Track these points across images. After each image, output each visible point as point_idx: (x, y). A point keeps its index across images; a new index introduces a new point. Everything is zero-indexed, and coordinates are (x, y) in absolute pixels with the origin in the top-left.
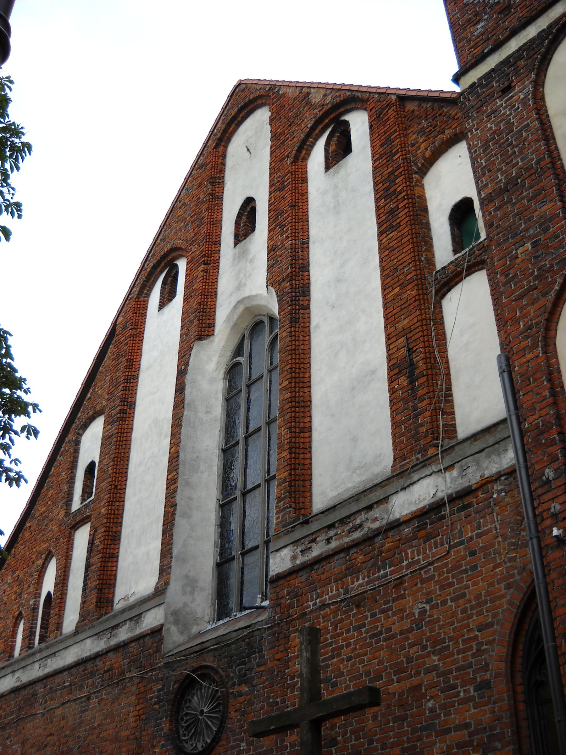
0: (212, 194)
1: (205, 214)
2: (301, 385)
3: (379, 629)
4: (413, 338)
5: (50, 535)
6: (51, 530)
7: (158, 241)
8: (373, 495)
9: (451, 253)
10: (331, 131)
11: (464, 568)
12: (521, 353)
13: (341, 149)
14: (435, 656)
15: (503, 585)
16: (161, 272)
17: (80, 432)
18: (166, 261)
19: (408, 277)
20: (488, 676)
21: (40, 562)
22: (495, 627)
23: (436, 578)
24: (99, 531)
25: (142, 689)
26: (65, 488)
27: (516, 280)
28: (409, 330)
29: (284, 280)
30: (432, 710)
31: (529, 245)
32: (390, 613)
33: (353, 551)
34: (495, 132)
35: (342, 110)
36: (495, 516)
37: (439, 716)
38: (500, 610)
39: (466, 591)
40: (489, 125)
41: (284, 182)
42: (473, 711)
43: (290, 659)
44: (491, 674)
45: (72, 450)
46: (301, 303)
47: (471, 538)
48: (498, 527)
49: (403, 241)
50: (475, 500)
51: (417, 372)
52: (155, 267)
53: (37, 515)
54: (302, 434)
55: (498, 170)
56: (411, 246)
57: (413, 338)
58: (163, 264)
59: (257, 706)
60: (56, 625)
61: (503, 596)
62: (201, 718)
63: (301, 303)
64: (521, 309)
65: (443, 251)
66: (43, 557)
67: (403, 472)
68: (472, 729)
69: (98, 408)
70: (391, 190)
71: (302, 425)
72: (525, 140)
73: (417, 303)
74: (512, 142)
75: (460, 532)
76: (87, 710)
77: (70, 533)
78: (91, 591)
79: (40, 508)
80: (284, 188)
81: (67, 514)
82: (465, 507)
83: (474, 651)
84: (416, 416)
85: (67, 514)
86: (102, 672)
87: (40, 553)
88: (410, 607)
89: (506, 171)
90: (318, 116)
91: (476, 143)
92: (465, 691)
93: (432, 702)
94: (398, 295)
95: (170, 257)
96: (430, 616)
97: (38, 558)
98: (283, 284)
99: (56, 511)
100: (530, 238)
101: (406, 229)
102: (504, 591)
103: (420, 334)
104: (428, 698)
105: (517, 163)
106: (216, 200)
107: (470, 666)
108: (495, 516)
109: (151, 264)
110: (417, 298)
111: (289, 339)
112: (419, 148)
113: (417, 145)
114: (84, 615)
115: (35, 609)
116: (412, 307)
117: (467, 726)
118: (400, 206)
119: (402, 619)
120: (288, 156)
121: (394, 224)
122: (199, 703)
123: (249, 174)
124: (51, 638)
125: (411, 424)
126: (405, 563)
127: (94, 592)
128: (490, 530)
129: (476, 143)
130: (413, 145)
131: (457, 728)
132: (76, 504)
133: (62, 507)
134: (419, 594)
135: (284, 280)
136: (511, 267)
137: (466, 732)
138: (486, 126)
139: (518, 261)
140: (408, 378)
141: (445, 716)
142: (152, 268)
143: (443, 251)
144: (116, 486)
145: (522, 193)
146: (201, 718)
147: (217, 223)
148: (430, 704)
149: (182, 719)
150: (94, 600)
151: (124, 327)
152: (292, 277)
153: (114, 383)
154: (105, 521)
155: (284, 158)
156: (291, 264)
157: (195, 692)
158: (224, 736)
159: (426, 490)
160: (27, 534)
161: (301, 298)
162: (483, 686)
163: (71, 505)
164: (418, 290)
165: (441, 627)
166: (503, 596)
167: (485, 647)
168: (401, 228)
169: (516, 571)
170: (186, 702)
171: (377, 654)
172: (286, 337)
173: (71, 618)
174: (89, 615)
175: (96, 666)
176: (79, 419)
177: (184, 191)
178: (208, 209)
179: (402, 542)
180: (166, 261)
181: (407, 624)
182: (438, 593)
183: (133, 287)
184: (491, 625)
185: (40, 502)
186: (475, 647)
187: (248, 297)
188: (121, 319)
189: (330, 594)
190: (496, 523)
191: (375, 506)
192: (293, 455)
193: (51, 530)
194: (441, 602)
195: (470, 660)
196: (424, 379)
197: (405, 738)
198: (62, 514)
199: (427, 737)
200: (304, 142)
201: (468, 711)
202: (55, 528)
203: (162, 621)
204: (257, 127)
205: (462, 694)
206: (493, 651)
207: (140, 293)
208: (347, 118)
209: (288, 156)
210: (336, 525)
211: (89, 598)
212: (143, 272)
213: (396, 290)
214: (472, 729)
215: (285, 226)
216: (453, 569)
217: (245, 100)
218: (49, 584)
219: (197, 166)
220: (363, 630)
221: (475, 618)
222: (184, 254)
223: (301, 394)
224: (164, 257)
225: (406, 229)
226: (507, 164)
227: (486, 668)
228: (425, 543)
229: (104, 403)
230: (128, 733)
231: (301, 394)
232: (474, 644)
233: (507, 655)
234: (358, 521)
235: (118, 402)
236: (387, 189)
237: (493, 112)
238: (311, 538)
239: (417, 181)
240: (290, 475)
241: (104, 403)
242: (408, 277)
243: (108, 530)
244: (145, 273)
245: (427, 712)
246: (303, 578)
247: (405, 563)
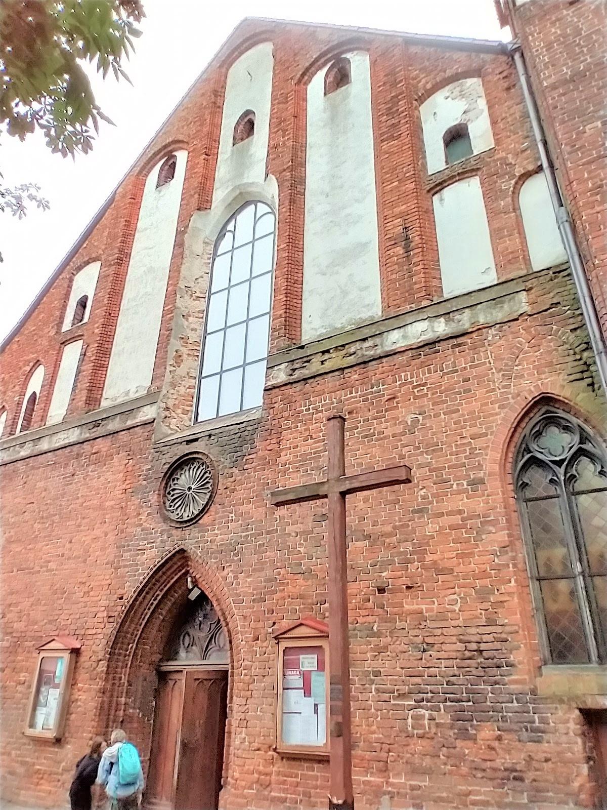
0: (215, 103)
1: (208, 117)
2: (296, 249)
3: (372, 431)
4: (409, 220)
5: (39, 348)
6: (41, 344)
7: (160, 134)
8: (368, 331)
9: (444, 164)
10: (332, 65)
11: (457, 390)
12: (591, 205)
13: (340, 78)
14: (427, 455)
15: (497, 406)
16: (160, 159)
17: (75, 273)
18: (166, 151)
19: (407, 175)
20: (481, 474)
21: (28, 368)
22: (489, 436)
23: (429, 396)
24: (91, 346)
25: (130, 469)
26: (58, 313)
27: (584, 149)
28: (406, 214)
29: (284, 170)
30: (423, 498)
31: (599, 124)
32: (383, 419)
33: (346, 371)
34: (560, 35)
35: (345, 48)
36: (489, 354)
37: (431, 503)
38: (494, 424)
39: (459, 408)
40: (553, 30)
41: (287, 98)
42: (466, 500)
43: (282, 450)
44: (485, 473)
45: (66, 285)
46: (298, 190)
47: (465, 368)
48: (492, 362)
49: (404, 148)
50: (469, 341)
51: (412, 244)
52: (155, 154)
53: (26, 332)
54: (296, 285)
55: (564, 65)
56: (411, 152)
57: (409, 220)
58: (162, 153)
59: (137, 502)
60: (40, 418)
61: (497, 414)
62: (188, 493)
63: (298, 190)
64: (589, 172)
65: (436, 159)
66: (31, 364)
67: (394, 318)
68: (466, 515)
69: (94, 255)
70: (395, 109)
71: (296, 278)
72: (596, 41)
73: (415, 194)
74: (579, 43)
75: (454, 362)
76: (71, 484)
77: (60, 347)
78: (81, 390)
79: (30, 327)
80: (288, 102)
81: (58, 332)
82: (459, 345)
83: (468, 454)
84: (411, 277)
85: (58, 332)
86: (89, 453)
87: (27, 362)
88: (402, 416)
89: (572, 66)
90: (323, 50)
91: (537, 44)
92: (458, 484)
93: (424, 490)
94: (397, 187)
95: (169, 149)
96: (422, 425)
97: (27, 362)
98: (284, 173)
99: (46, 331)
100: (600, 118)
101: (407, 140)
102: (497, 410)
103: (417, 217)
104: (420, 487)
105: (586, 60)
106: (217, 107)
107: (463, 465)
108: (489, 354)
109: (153, 152)
110: (415, 190)
111: (288, 214)
112: (420, 81)
113: (418, 79)
114: (71, 410)
115: (19, 404)
116: (410, 196)
117: (460, 512)
118: (402, 122)
119: (395, 424)
120: (292, 79)
121: (395, 135)
122: (186, 479)
123: (252, 89)
124: (34, 427)
125: (405, 282)
126: (398, 383)
127: (85, 392)
128: (485, 363)
129: (537, 44)
130: (414, 79)
131: (450, 513)
132: (67, 326)
133: (52, 327)
134: (412, 407)
135: (284, 170)
136: (577, 139)
137: (459, 517)
138: (551, 31)
139: (586, 135)
140: (404, 248)
141: (437, 502)
142: (153, 154)
143: (436, 159)
144: (110, 314)
145: (591, 83)
146: (188, 493)
147: (216, 126)
148: (422, 493)
149: (169, 493)
150: (84, 399)
151: (124, 196)
152: (292, 169)
153: (112, 237)
154: (99, 338)
155: (288, 80)
156: (292, 160)
157: (183, 472)
158: (213, 508)
159: (420, 330)
160: (15, 346)
161: (299, 186)
162: (476, 483)
163: (61, 327)
164: (416, 185)
165: (434, 434)
166: (497, 414)
167: (478, 451)
168: (401, 139)
169: (510, 396)
170: (173, 480)
171: (369, 451)
172: (286, 212)
173: (58, 410)
174: (77, 409)
175: (83, 449)
176: (74, 263)
177: (187, 98)
178: (211, 113)
179: (396, 367)
180: (166, 151)
181: (400, 429)
182: (431, 407)
183: (134, 167)
184: (486, 435)
185: (30, 322)
186: (468, 450)
187: (244, 184)
188: (120, 190)
189: (323, 402)
190: (490, 359)
191: (369, 339)
192: (289, 299)
193: (41, 344)
194: (434, 415)
195: (464, 460)
196: (420, 250)
197: (397, 518)
198: (52, 333)
199: (419, 518)
200: (307, 69)
201: (462, 500)
202: (45, 343)
203: (154, 416)
204: (259, 63)
205: (455, 486)
206: (487, 455)
207: (140, 172)
208: (348, 56)
209: (292, 79)
210: (331, 351)
211: (78, 397)
212: (144, 157)
213: (394, 184)
214: (466, 515)
215: (287, 130)
216: (446, 390)
217: (247, 38)
218: (35, 384)
219: (203, 80)
220: (355, 431)
221: (468, 428)
222: (185, 146)
223: (296, 256)
224: (165, 147)
225: (407, 140)
226: (574, 60)
227: (480, 467)
228: (418, 369)
229: (101, 252)
230: (113, 503)
231: (296, 256)
232: (467, 449)
233: (501, 459)
234: (353, 350)
235: (116, 251)
236: (390, 109)
237: (558, 20)
238: (305, 359)
239: (416, 107)
240: (286, 312)
241: (101, 252)
242: (407, 175)
243: (101, 345)
244: (145, 159)
245: (420, 499)
246: (298, 389)
247: (398, 383)
